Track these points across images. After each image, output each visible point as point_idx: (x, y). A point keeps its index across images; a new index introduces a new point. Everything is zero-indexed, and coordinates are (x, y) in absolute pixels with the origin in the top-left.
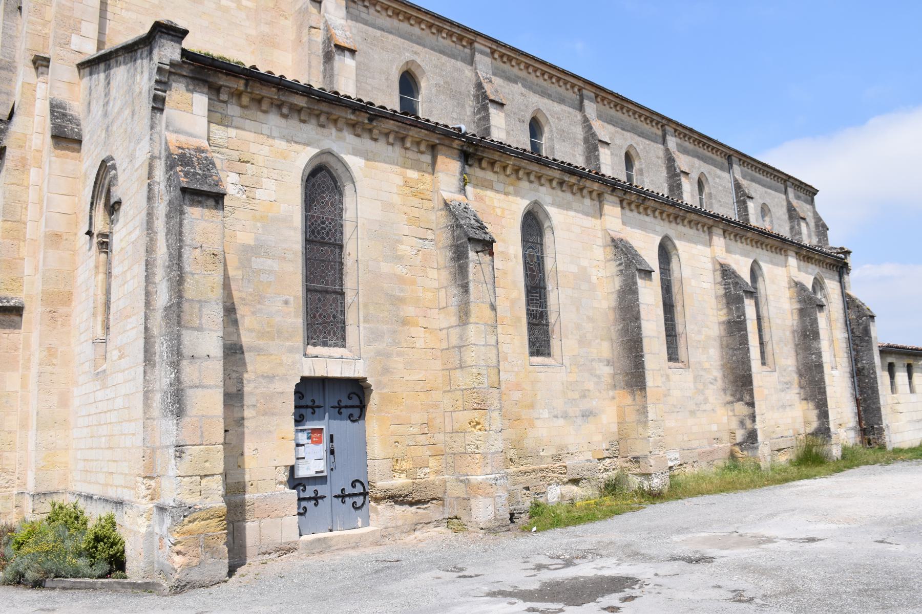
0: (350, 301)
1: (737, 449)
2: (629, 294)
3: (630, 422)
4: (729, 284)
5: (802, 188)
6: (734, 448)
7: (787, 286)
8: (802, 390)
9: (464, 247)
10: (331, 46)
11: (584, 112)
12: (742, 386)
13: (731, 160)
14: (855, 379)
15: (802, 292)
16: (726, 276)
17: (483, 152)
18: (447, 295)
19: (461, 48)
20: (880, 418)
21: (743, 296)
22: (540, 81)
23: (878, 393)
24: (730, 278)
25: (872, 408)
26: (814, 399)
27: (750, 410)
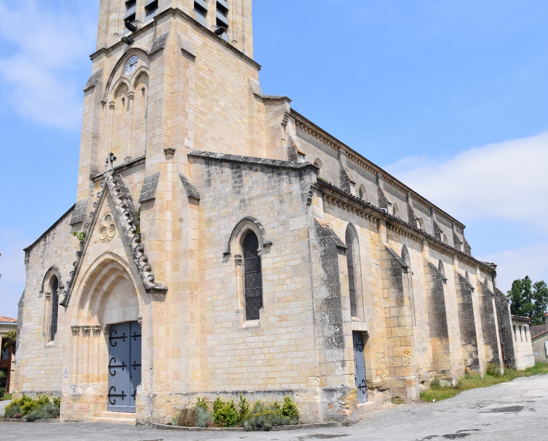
0: (359, 295)
1: (468, 368)
2: (438, 291)
3: (440, 354)
4: (463, 285)
5: (459, 225)
6: (466, 368)
7: (476, 284)
8: (484, 339)
9: (399, 270)
10: (295, 152)
11: (379, 185)
12: (471, 336)
13: (432, 210)
14: (501, 334)
15: (484, 288)
16: (462, 280)
17: (392, 222)
18: (388, 292)
19: (334, 150)
20: (513, 354)
21: (470, 291)
22: (364, 170)
23: (512, 341)
24: (464, 282)
25: (509, 349)
26: (491, 344)
27: (475, 348)
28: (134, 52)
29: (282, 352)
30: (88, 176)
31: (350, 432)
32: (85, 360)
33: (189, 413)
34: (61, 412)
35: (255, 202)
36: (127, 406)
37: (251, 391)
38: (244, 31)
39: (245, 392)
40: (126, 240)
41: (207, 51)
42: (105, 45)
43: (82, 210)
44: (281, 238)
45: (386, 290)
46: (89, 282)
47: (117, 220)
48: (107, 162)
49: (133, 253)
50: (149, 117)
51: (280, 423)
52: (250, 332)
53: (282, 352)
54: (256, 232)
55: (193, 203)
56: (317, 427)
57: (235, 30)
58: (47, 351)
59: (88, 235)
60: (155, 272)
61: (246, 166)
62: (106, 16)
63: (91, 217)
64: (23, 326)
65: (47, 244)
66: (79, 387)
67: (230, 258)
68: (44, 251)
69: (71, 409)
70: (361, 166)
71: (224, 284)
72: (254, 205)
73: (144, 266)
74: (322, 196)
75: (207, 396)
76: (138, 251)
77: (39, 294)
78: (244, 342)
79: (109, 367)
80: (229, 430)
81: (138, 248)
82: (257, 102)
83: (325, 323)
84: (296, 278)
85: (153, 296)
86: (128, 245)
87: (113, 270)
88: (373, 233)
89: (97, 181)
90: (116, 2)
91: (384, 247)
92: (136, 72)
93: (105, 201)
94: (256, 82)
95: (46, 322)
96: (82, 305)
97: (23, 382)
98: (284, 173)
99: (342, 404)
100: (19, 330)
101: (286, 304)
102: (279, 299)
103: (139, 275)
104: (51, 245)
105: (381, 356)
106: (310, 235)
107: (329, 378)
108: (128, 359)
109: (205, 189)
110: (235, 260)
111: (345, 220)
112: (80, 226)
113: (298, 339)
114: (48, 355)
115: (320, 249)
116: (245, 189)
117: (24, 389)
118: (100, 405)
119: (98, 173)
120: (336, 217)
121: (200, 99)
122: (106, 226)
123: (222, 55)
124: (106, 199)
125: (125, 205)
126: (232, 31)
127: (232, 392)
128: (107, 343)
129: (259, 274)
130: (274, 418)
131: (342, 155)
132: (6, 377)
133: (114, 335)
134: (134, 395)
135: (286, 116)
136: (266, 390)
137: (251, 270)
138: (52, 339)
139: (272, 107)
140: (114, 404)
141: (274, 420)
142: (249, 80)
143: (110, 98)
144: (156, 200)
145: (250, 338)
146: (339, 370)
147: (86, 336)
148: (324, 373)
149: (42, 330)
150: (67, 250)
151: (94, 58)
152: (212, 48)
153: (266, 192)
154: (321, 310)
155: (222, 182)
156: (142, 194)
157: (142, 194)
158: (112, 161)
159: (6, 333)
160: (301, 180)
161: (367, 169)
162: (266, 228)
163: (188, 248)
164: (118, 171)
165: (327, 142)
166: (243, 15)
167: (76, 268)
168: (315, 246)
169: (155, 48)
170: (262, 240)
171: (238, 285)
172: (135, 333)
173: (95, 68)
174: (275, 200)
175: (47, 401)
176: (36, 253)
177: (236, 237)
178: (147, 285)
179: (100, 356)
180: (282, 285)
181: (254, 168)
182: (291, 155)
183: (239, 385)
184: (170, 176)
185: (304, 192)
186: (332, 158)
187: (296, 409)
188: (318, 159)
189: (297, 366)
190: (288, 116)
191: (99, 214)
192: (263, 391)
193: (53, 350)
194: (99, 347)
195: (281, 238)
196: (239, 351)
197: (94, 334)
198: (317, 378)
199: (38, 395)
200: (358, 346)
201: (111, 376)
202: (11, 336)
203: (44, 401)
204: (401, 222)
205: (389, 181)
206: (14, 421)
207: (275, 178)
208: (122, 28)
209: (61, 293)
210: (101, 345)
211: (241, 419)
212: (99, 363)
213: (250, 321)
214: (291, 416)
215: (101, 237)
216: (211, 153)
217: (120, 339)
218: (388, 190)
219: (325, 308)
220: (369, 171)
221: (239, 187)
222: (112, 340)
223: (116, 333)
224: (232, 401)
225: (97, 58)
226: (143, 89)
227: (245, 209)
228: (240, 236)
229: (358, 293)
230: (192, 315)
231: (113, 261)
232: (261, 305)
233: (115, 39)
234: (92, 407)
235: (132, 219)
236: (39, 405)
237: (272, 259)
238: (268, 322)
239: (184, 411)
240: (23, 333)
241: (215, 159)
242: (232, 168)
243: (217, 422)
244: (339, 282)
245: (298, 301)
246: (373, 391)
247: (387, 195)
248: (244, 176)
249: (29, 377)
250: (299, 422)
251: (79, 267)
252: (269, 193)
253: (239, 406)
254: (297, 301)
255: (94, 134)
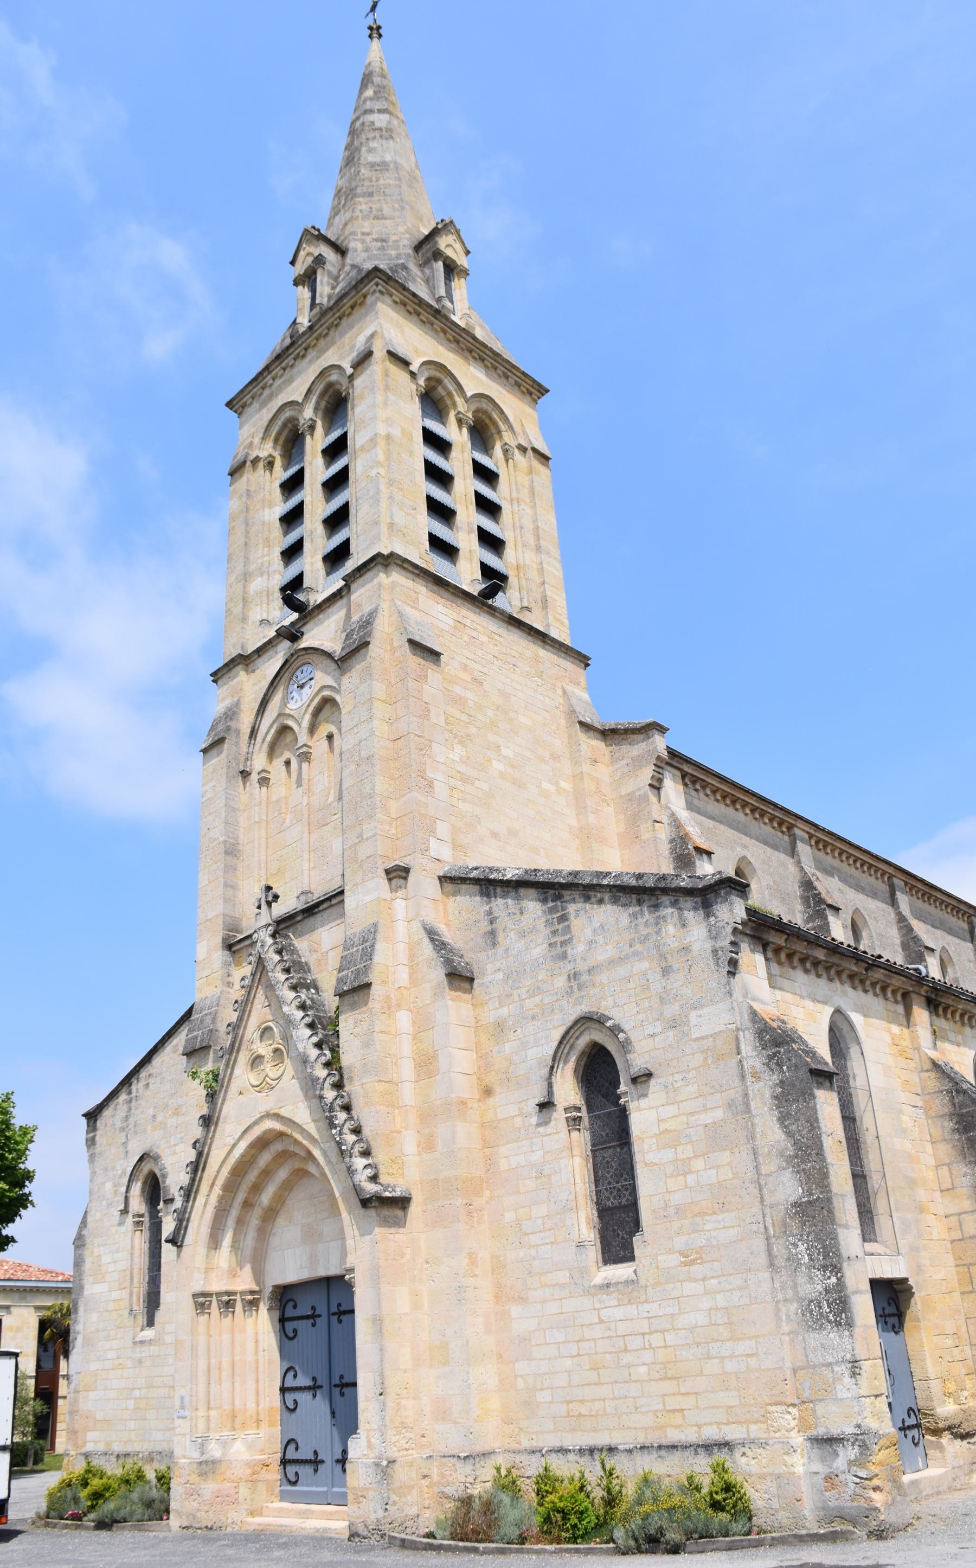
0: (876, 1186)
10: (687, 848)
17: (942, 996)
18: (951, 1174)
19: (779, 834)
22: (857, 874)
28: (306, 656)
29: (698, 1344)
30: (219, 939)
31: (890, 1558)
32: (226, 1373)
33: (476, 1505)
34: (173, 1505)
35: (603, 977)
36: (325, 1489)
37: (627, 1447)
38: (543, 583)
39: (611, 1450)
40: (310, 1083)
41: (465, 638)
42: (242, 647)
43: (208, 1019)
44: (672, 1060)
45: (946, 1168)
46: (231, 1187)
47: (287, 1038)
48: (259, 907)
49: (327, 1114)
50: (346, 797)
51: (707, 1532)
52: (615, 1295)
53: (698, 1344)
54: (612, 1047)
55: (456, 989)
56: (801, 1541)
57: (524, 583)
58: (139, 1352)
59: (224, 1076)
60: (380, 1156)
61: (576, 894)
62: (240, 585)
63: (228, 1034)
64: (86, 1293)
65: (134, 1100)
66: (214, 1441)
67: (555, 1115)
68: (127, 1117)
69: (196, 1496)
70: (849, 865)
71: (543, 1179)
72: (601, 984)
73: (354, 1144)
74: (761, 949)
75: (518, 1461)
76: (338, 1108)
77: (118, 1218)
78: (601, 1321)
79: (281, 1390)
80: (577, 1551)
81: (339, 1101)
82: (589, 741)
83: (799, 1265)
84: (717, 1154)
85: (378, 1215)
86: (315, 1096)
87: (284, 1156)
88: (896, 1029)
89: (238, 950)
90: (260, 555)
91: (928, 1062)
92: (312, 700)
93: (257, 995)
94: (581, 694)
95: (136, 1284)
96: (214, 1241)
97: (86, 1430)
98: (668, 902)
99: (861, 1478)
100: (77, 1303)
101: (698, 1219)
102: (678, 1209)
103: (343, 1165)
104: (143, 1102)
105: (949, 1342)
106: (743, 1047)
107: (820, 1408)
108: (326, 1372)
109: (483, 954)
110: (567, 1119)
111: (825, 1003)
112: (205, 1055)
113: (735, 1307)
114: (140, 1361)
115: (770, 1080)
116: (578, 949)
117: (89, 1447)
118: (262, 1488)
119: (240, 932)
120: (802, 997)
121: (458, 748)
122: (263, 1053)
123: (501, 643)
124: (262, 992)
125: (305, 1002)
126: (517, 588)
127: (580, 1450)
128: (275, 1332)
129: (626, 1149)
130: (689, 1517)
131: (800, 845)
132: (48, 1414)
133: (290, 1312)
134: (343, 1461)
135: (659, 767)
136: (664, 1442)
137: (605, 1142)
138: (151, 1323)
139: (625, 748)
140: (294, 1483)
141: (688, 1523)
142: (565, 692)
143: (259, 761)
144: (373, 987)
145: (615, 1310)
146: (845, 1387)
147: (227, 1316)
148: (806, 1395)
149: (127, 1302)
150: (177, 1112)
151: (219, 678)
152: (475, 630)
153: (627, 950)
154: (785, 1232)
155: (522, 934)
156: (340, 975)
157: (340, 975)
158: (269, 904)
159: (48, 1308)
160: (708, 915)
161: (864, 872)
162: (633, 1036)
163: (453, 1096)
164: (283, 925)
165: (762, 816)
166: (538, 549)
167: (200, 1154)
168: (756, 1073)
169: (350, 644)
170: (628, 1066)
171: (578, 1180)
172: (339, 1305)
173: (223, 699)
174: (650, 969)
175: (140, 1476)
176: (110, 1122)
177: (566, 1062)
178: (362, 1190)
179: (261, 1363)
180: (685, 1174)
181: (595, 896)
182: (678, 856)
183: (595, 1430)
184: (401, 929)
185: (719, 944)
186: (776, 852)
187: (742, 1491)
188: (743, 859)
189: (738, 1378)
190: (663, 765)
191: (245, 1027)
192: (656, 1445)
193: (153, 1350)
194: (257, 1342)
195: (672, 1060)
196: (591, 1344)
197: (245, 1311)
198: (791, 1409)
199: (121, 1462)
200: (888, 1319)
201: (288, 1414)
202: (59, 1315)
203: (133, 1477)
204: (963, 994)
205: (923, 895)
206: (66, 1526)
207: (647, 916)
208: (277, 608)
209: (167, 1213)
210: (260, 1337)
211: (605, 1522)
212: (257, 1382)
213: (613, 1267)
214: (733, 1511)
215: (254, 1079)
216: (491, 870)
217: (305, 1321)
218: (921, 917)
219: (794, 1226)
220: (870, 875)
221: (563, 943)
222: (287, 1324)
223: (295, 1307)
224: (580, 1472)
225: (227, 676)
226: (330, 737)
227: (582, 994)
228: (573, 1059)
229: (874, 1181)
230: (473, 1261)
231: (281, 1135)
232: (636, 1226)
233: (262, 632)
234: (244, 1491)
235: (320, 1035)
236: (124, 1488)
237: (654, 1111)
238: (657, 1267)
239: (463, 1502)
240: (85, 1311)
241: (502, 881)
242: (544, 901)
243: (545, 1528)
244: (823, 1160)
245: (727, 1211)
246: (941, 1437)
247: (919, 928)
248: (572, 917)
249: (100, 1416)
250: (755, 1529)
251: (205, 1152)
252: (635, 954)
253: (599, 1485)
254: (724, 1212)
255: (228, 845)
